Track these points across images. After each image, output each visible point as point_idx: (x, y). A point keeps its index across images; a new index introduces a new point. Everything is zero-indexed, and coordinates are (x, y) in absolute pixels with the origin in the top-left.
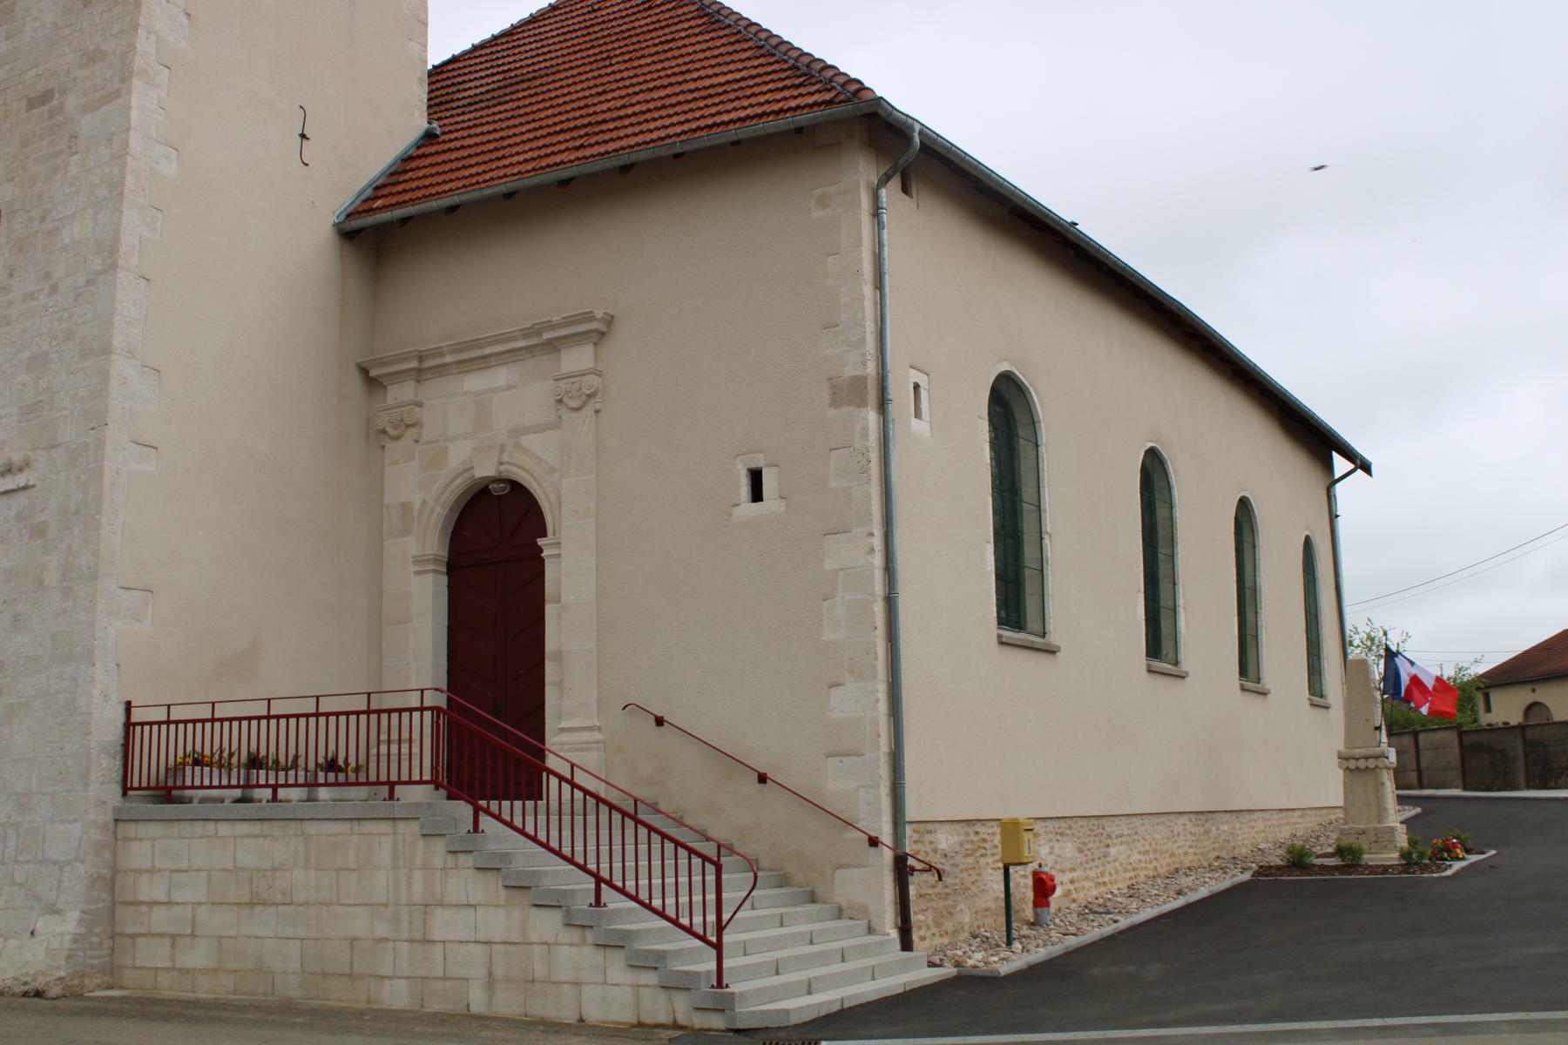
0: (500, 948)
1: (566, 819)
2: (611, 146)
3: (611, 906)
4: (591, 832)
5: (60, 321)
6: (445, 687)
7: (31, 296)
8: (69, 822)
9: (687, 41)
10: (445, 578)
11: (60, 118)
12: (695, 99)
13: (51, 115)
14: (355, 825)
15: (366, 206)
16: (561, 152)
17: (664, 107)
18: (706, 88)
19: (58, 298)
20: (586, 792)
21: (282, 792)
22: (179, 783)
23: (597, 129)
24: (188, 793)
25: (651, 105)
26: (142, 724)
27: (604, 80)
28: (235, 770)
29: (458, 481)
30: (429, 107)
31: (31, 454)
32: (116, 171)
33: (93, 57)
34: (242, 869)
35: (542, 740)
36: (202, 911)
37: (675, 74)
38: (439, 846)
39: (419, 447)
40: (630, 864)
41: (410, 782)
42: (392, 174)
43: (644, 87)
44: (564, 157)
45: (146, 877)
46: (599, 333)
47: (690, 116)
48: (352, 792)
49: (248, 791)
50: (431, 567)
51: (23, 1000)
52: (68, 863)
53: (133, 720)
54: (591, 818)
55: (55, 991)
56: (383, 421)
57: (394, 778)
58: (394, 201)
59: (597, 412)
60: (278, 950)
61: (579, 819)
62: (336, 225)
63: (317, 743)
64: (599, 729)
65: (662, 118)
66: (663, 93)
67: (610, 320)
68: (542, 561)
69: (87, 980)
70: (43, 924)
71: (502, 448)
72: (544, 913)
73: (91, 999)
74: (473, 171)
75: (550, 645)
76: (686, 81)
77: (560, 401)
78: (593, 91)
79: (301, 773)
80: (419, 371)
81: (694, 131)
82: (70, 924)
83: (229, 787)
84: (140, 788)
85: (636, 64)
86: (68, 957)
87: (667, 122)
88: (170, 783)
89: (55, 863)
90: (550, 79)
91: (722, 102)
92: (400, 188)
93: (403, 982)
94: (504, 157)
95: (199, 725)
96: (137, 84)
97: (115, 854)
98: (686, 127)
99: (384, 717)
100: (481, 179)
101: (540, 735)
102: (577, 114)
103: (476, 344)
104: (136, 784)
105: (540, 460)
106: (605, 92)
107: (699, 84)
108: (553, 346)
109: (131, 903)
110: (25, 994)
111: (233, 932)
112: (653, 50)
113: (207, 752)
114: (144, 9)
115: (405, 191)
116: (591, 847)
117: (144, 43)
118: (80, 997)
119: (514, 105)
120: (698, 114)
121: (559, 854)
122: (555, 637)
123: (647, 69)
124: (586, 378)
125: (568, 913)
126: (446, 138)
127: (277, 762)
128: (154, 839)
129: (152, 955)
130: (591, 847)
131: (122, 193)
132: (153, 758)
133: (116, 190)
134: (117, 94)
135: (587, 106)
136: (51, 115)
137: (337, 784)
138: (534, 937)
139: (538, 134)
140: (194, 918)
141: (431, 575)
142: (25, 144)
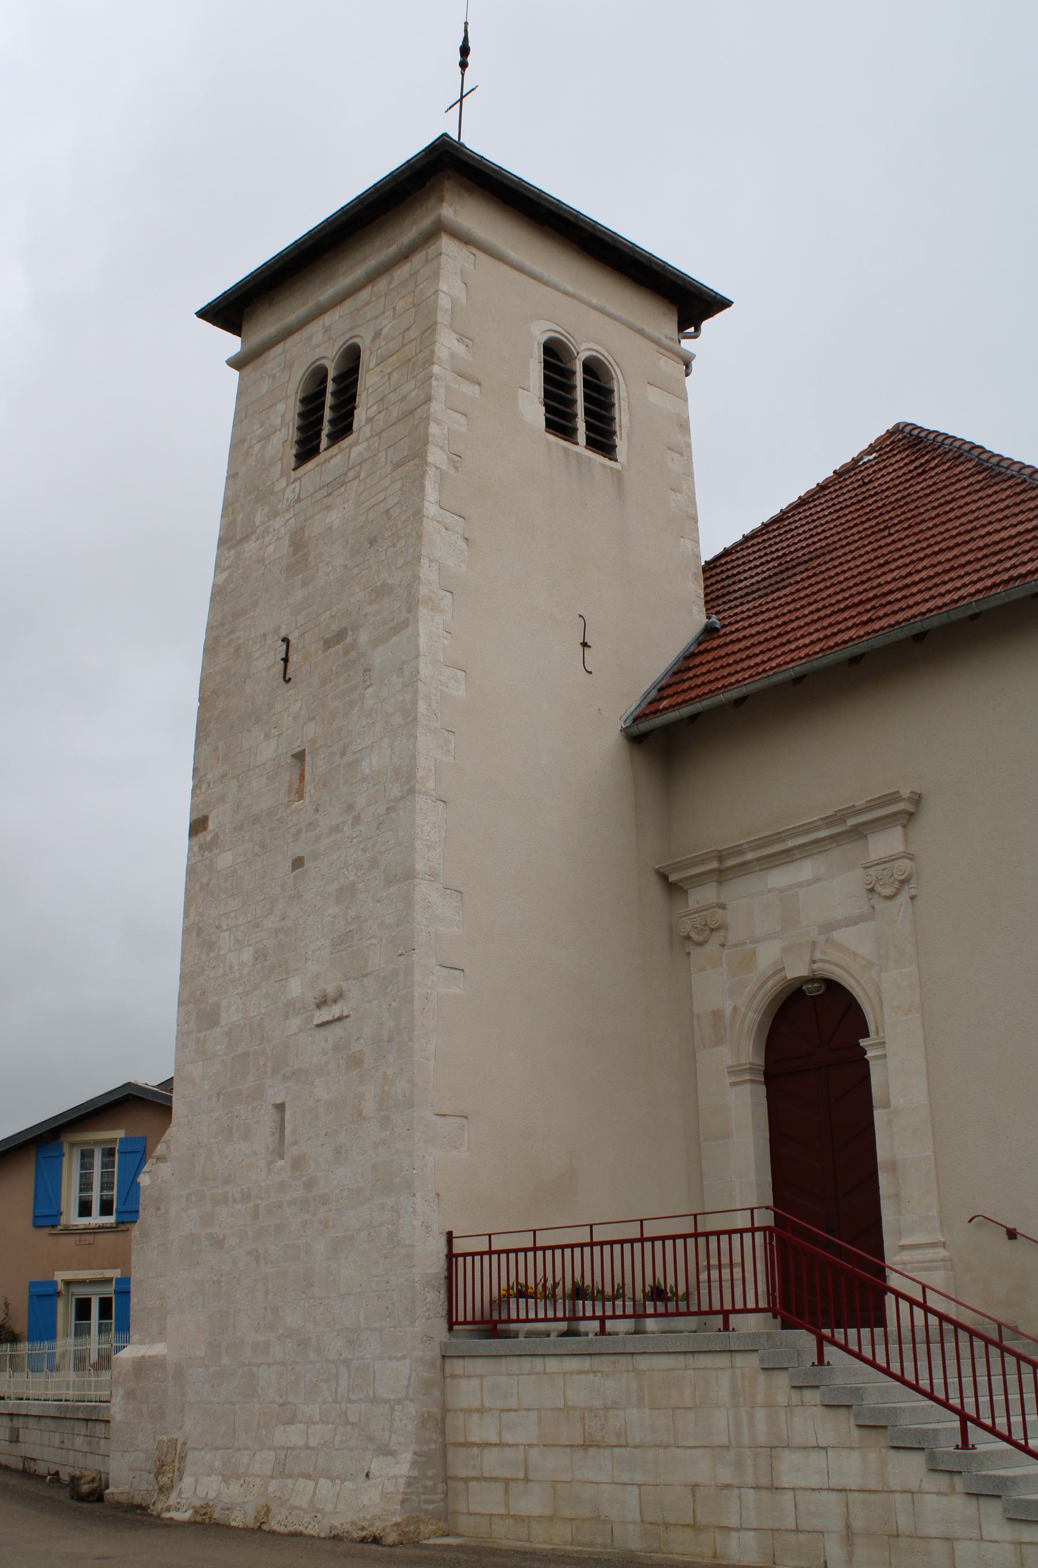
0: (857, 1496)
1: (907, 1347)
2: (900, 617)
3: (981, 1448)
4: (952, 1363)
5: (364, 850)
6: (771, 1203)
7: (336, 829)
8: (398, 1359)
9: (968, 499)
10: (764, 1088)
11: (353, 654)
12: (986, 556)
13: (346, 652)
14: (690, 1360)
15: (652, 708)
16: (848, 629)
17: (953, 569)
18: (996, 543)
19: (362, 828)
20: (942, 1318)
21: (609, 1324)
22: (504, 1316)
23: (883, 601)
24: (513, 1326)
25: (939, 569)
26: (465, 1255)
27: (885, 551)
28: (560, 1301)
29: (770, 984)
30: (706, 602)
31: (344, 984)
32: (408, 698)
33: (381, 592)
34: (573, 1408)
35: (881, 1256)
36: (534, 1453)
37: (960, 534)
38: (782, 1381)
39: (726, 951)
40: (999, 1398)
41: (746, 1311)
42: (675, 674)
43: (928, 551)
44: (852, 633)
45: (475, 1416)
46: (907, 814)
47: (982, 574)
48: (680, 1323)
49: (574, 1323)
50: (747, 1077)
51: (361, 1545)
52: (399, 1402)
53: (455, 1251)
54: (950, 1346)
55: (392, 1537)
56: (686, 926)
57: (728, 1306)
58: (680, 700)
59: (912, 898)
60: (615, 1497)
61: (935, 1348)
62: (623, 730)
63: (640, 1271)
64: (944, 1245)
65: (952, 580)
66: (950, 555)
67: (917, 799)
68: (866, 1063)
69: (422, 1527)
70: (377, 1465)
71: (814, 945)
72: (904, 1455)
73: (427, 1547)
74: (758, 660)
75: (882, 1154)
76: (973, 539)
77: (872, 890)
78: (875, 564)
79: (629, 1304)
80: (720, 871)
81: (990, 588)
82: (402, 1467)
83: (555, 1319)
84: (465, 1323)
85: (916, 529)
86: (403, 1501)
87: (958, 583)
88: (495, 1317)
89: (387, 1401)
90: (828, 558)
91: (1016, 555)
92: (685, 686)
93: (752, 1534)
94: (789, 642)
95: (669, 1243)
96: (423, 612)
97: (443, 1393)
98: (979, 586)
99: (713, 1240)
100: (767, 666)
101: (878, 1250)
102: (861, 588)
103: (778, 837)
104: (461, 1319)
105: (855, 954)
106: (887, 563)
107: (988, 540)
108: (859, 833)
109: (462, 1445)
110: (363, 1540)
111: (566, 1477)
112: (933, 514)
113: (531, 1283)
114: (425, 539)
115: (691, 688)
116: (953, 1380)
117: (427, 572)
118: (416, 1544)
119: (793, 589)
120: (991, 571)
121: (916, 1388)
122: (887, 1145)
123: (929, 534)
124: (898, 863)
125: (932, 1458)
126: (727, 630)
127: (602, 1292)
128: (482, 1377)
129: (483, 1501)
130: (953, 1380)
131: (415, 719)
132: (479, 1288)
133: (410, 715)
134: (406, 623)
135: (870, 579)
136: (346, 652)
137: (667, 1315)
138: (894, 1484)
139: (822, 614)
140: (526, 1460)
141: (748, 1086)
142: (323, 683)
